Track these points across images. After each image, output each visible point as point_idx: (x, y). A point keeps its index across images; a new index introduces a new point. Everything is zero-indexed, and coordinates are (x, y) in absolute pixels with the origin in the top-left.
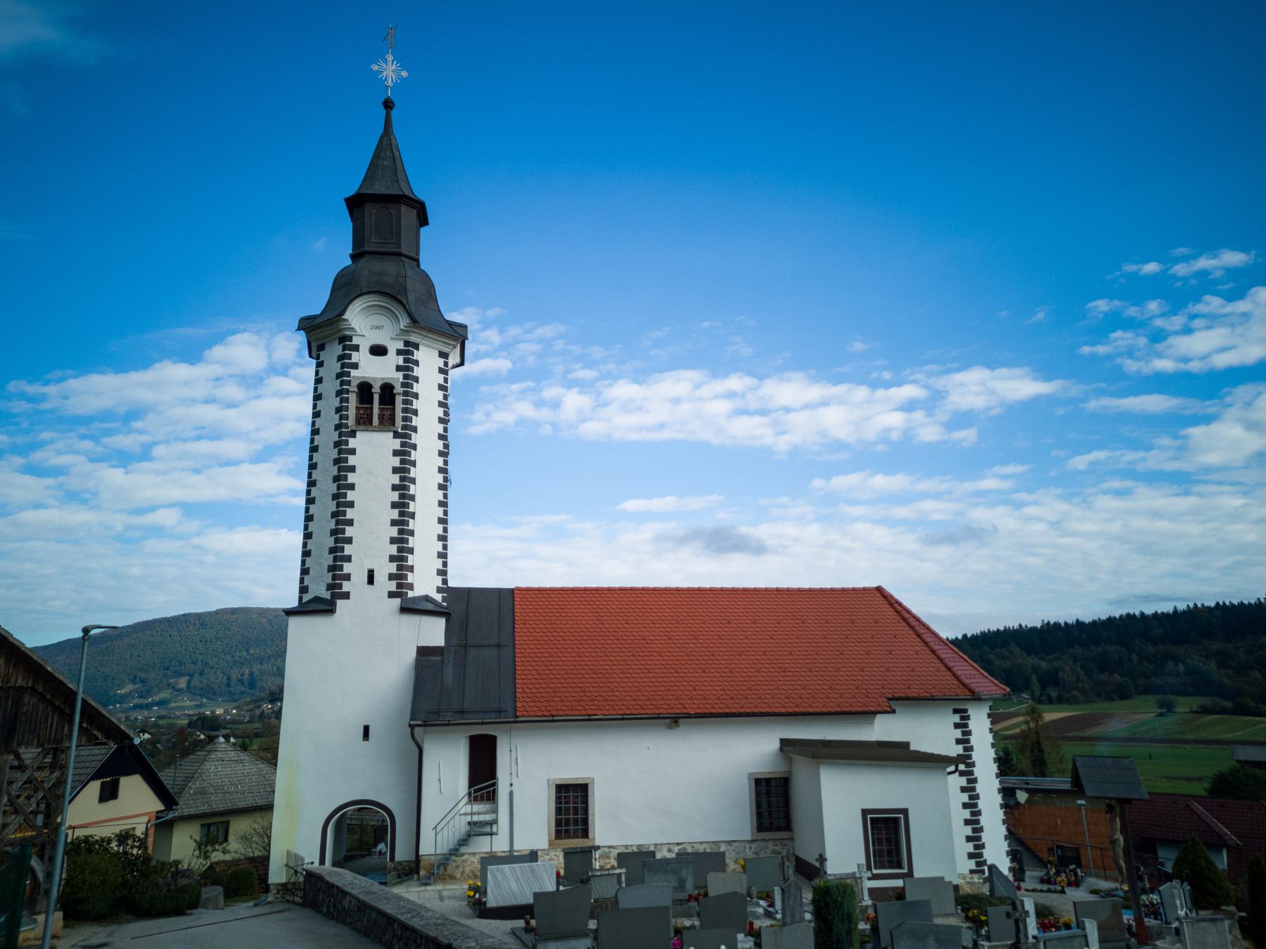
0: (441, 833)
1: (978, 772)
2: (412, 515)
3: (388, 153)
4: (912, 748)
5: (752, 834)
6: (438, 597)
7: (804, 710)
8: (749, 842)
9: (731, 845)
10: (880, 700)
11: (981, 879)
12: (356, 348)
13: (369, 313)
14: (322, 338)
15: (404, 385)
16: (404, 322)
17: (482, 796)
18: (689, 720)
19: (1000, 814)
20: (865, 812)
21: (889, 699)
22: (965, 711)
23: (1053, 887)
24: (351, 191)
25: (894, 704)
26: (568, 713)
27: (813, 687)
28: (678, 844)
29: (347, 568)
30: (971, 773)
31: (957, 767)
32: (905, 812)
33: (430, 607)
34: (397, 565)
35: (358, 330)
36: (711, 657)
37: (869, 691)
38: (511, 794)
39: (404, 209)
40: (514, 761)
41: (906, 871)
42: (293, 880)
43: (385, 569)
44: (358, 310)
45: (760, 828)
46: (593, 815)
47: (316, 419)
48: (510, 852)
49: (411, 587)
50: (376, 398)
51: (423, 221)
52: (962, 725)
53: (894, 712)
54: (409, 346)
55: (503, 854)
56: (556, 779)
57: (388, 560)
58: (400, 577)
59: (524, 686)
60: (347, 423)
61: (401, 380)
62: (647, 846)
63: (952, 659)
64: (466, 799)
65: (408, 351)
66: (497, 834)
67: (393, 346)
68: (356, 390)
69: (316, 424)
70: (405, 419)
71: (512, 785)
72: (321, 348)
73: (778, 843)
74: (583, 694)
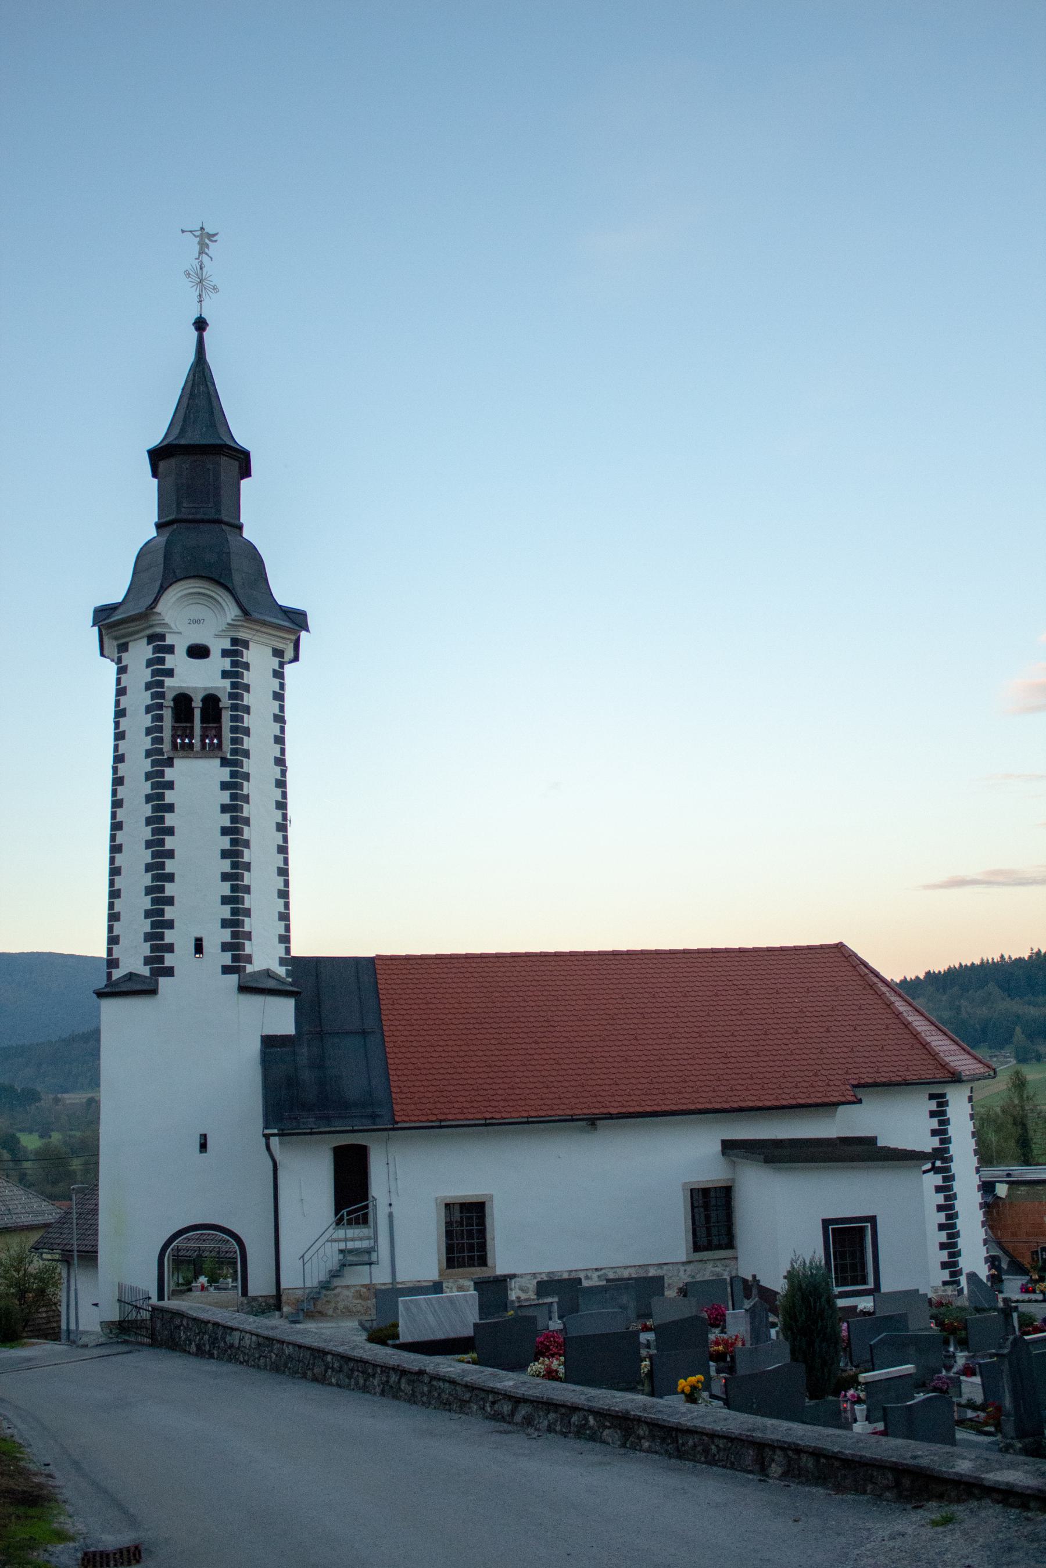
0: (310, 1262)
1: (955, 1167)
2: (247, 867)
3: (202, 388)
4: (880, 1144)
5: (687, 1254)
6: (281, 971)
7: (751, 1104)
8: (683, 1263)
9: (662, 1268)
10: (843, 1088)
11: (955, 1290)
12: (171, 649)
13: (191, 601)
14: (124, 636)
15: (232, 696)
16: (232, 611)
17: (357, 1219)
18: (610, 1121)
19: (980, 1215)
20: (826, 1223)
21: (854, 1086)
22: (943, 1095)
23: (1033, 1296)
24: (156, 437)
25: (860, 1093)
26: (459, 1116)
27: (761, 1076)
28: (596, 1269)
29: (169, 936)
30: (948, 1169)
31: (933, 1164)
32: (872, 1220)
33: (272, 984)
34: (232, 932)
35: (173, 625)
36: (633, 1042)
37: (830, 1077)
38: (391, 1216)
39: (224, 460)
40: (392, 1177)
41: (871, 1285)
42: (132, 1317)
43: (216, 936)
44: (174, 599)
45: (697, 1248)
46: (493, 1239)
47: (120, 742)
48: (392, 1283)
49: (249, 959)
50: (197, 713)
51: (246, 472)
52: (939, 1114)
53: (860, 1101)
54: (237, 645)
55: (383, 1287)
56: (445, 1197)
57: (219, 925)
58: (235, 947)
59: (401, 1084)
60: (162, 748)
61: (229, 690)
62: (559, 1273)
63: (928, 1033)
64: (334, 1225)
65: (235, 651)
66: (378, 1264)
67: (217, 645)
68: (172, 704)
69: (120, 748)
70: (234, 741)
71: (390, 1205)
72: (123, 648)
73: (718, 1263)
74: (476, 1093)
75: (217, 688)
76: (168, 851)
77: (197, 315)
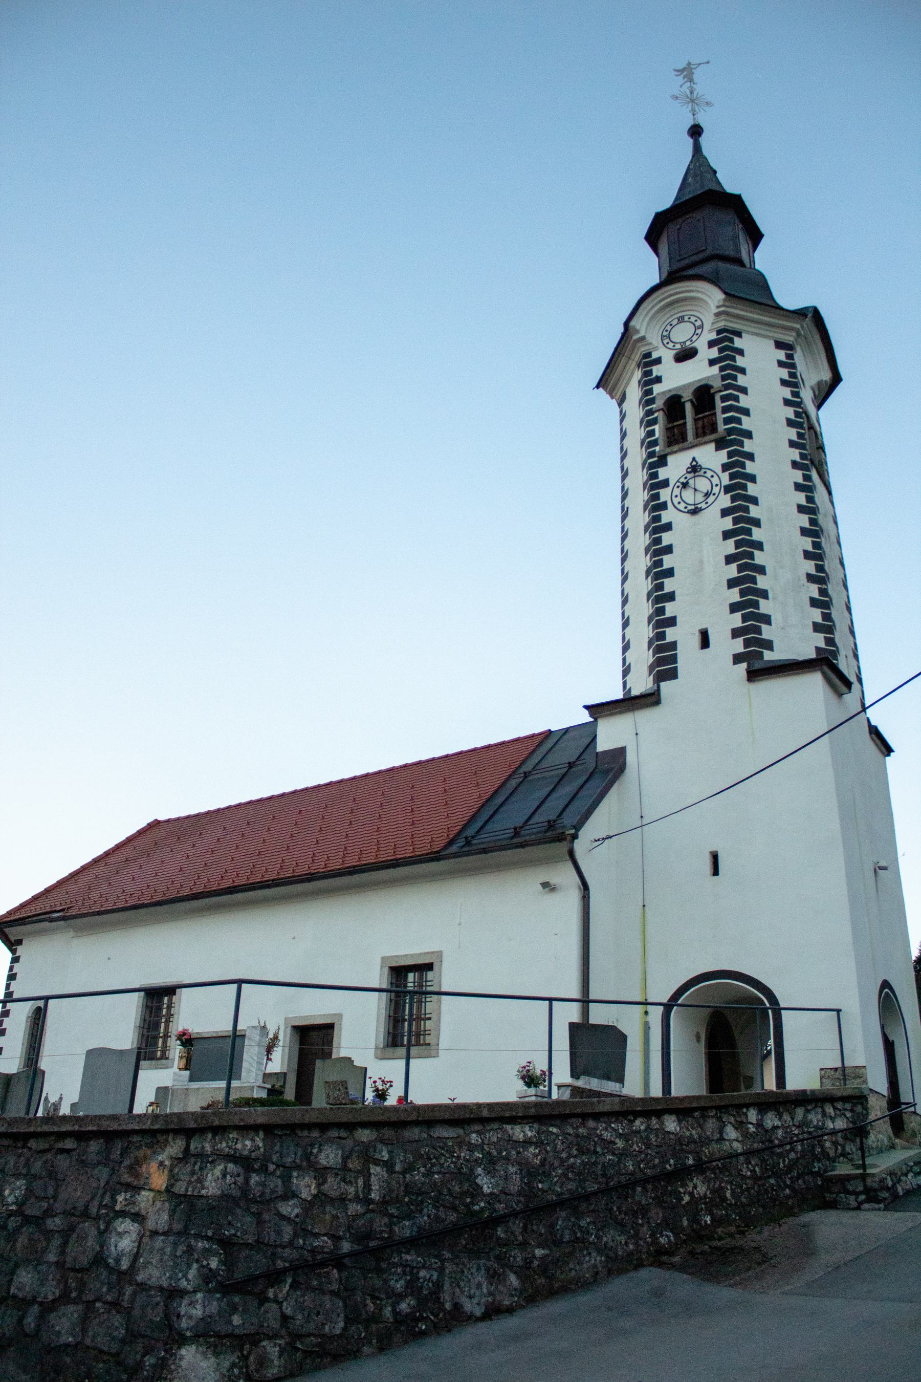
75: (708, 378)
76: (738, 637)
77: (691, 123)
